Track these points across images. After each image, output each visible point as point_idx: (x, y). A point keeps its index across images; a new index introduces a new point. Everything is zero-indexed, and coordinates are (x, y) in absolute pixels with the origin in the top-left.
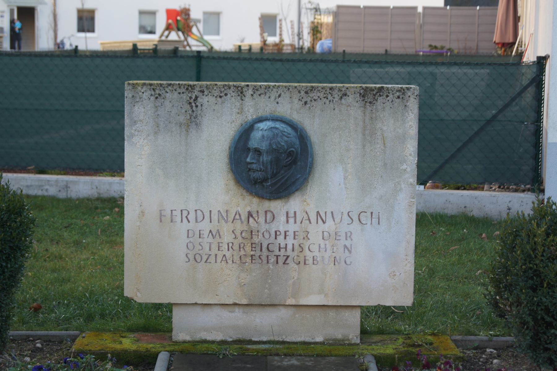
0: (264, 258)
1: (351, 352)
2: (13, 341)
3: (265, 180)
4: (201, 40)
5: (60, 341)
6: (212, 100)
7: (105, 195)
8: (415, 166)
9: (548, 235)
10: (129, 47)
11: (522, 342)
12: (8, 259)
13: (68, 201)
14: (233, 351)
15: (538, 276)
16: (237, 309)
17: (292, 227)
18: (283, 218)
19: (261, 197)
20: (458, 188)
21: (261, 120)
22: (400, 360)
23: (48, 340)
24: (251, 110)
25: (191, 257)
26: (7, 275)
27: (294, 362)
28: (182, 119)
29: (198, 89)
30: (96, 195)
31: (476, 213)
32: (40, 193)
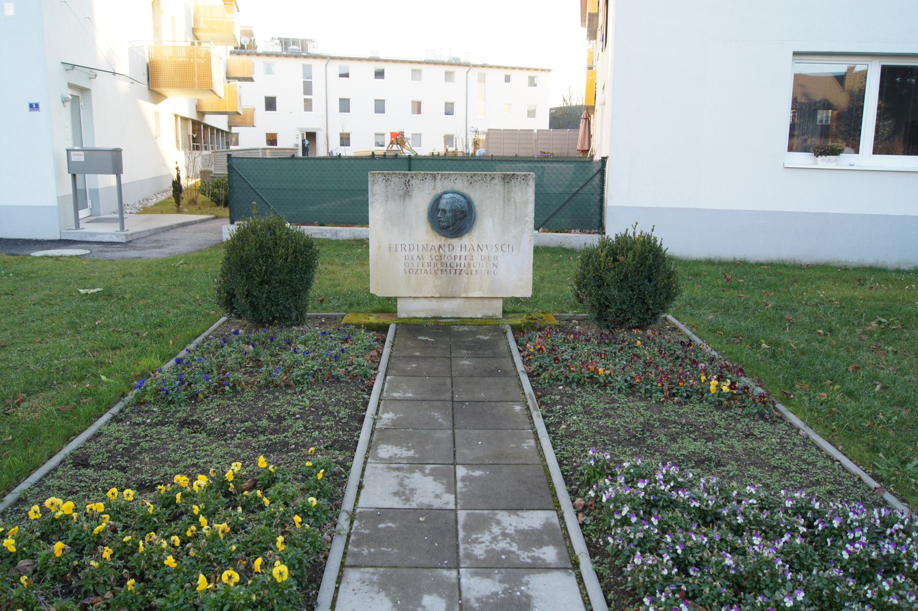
0: (448, 271)
1: (497, 323)
2: (309, 318)
3: (449, 227)
4: (410, 150)
5: (335, 318)
6: (418, 181)
7: (358, 238)
8: (533, 218)
9: (607, 256)
10: (370, 154)
11: (41, 504)
12: (305, 273)
13: (338, 241)
14: (432, 323)
15: (601, 279)
16: (433, 299)
17: (464, 253)
18: (459, 248)
19: (446, 236)
20: (557, 232)
21: (445, 193)
22: (524, 327)
23: (328, 318)
24: (440, 187)
25: (407, 271)
26: (305, 282)
27: (466, 328)
28: (401, 192)
29: (410, 175)
30: (353, 238)
31: (567, 246)
32: (321, 237)
